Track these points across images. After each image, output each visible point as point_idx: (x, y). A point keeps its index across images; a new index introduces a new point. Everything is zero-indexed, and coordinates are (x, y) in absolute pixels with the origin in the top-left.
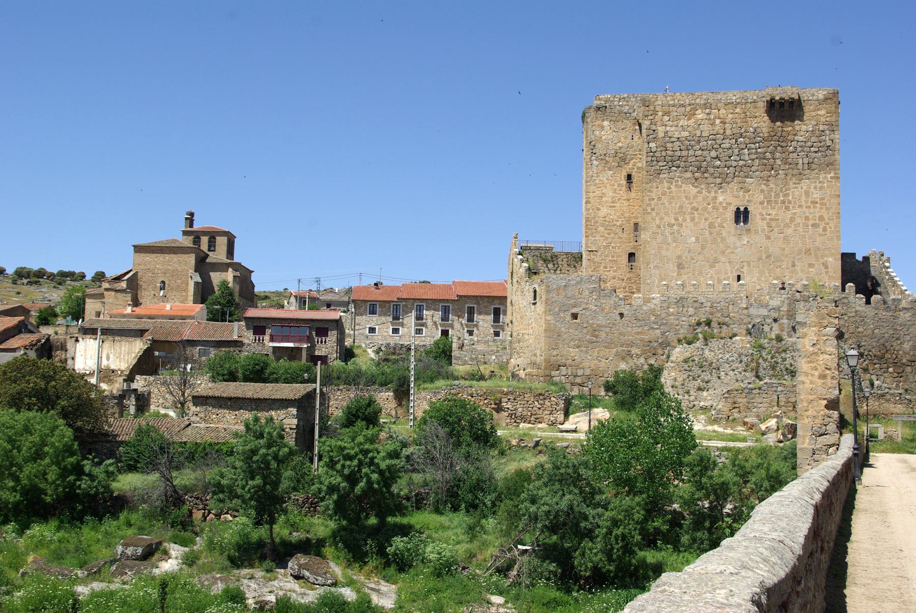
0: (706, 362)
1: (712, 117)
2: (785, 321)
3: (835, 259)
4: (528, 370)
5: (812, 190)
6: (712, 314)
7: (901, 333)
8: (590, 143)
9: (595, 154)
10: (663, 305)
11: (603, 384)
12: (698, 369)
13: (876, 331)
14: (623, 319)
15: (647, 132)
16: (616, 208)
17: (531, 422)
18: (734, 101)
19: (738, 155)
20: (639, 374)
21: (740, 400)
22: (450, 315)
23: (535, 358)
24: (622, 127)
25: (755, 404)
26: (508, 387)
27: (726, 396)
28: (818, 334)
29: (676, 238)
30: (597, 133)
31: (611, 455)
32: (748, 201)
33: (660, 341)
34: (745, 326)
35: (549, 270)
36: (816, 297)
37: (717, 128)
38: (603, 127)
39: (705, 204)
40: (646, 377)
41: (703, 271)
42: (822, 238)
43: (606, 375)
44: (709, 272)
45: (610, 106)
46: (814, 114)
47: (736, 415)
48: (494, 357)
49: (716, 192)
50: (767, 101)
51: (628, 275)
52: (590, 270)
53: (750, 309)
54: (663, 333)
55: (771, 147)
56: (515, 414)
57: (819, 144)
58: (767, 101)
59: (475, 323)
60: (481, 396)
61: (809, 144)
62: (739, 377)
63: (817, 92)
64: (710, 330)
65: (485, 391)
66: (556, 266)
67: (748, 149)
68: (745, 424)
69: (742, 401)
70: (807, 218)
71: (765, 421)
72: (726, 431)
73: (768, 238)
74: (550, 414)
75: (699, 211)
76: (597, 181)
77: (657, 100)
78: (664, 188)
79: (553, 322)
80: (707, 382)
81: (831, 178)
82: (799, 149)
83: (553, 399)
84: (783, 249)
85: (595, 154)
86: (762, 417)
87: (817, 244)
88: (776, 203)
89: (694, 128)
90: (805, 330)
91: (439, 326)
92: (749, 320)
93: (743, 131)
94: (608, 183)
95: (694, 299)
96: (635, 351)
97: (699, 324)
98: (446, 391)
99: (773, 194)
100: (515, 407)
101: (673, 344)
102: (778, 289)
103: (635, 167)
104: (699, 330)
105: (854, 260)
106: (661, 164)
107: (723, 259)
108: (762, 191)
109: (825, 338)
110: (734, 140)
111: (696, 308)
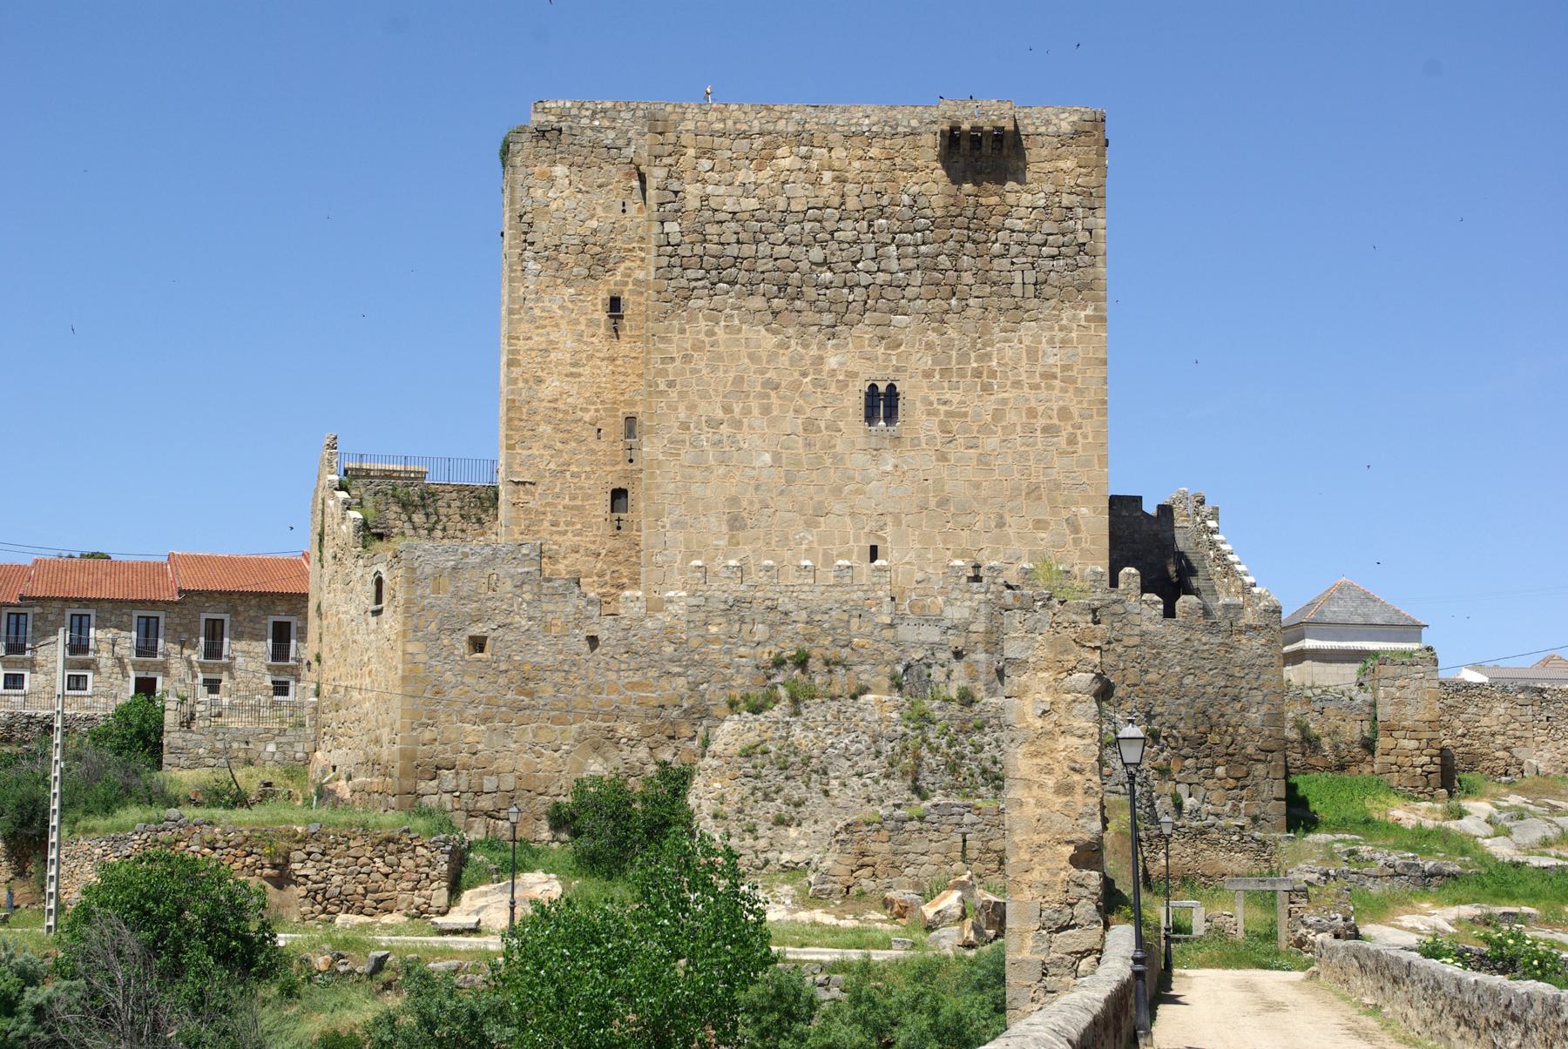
0: (796, 754)
1: (814, 164)
2: (981, 656)
5: (1044, 345)
7: (1244, 683)
8: (521, 217)
11: (547, 813)
13: (1188, 680)
14: (597, 650)
15: (658, 196)
16: (583, 378)
18: (865, 129)
19: (873, 259)
20: (635, 785)
21: (875, 847)
22: (161, 641)
23: (376, 749)
24: (600, 181)
25: (910, 856)
26: (308, 822)
27: (842, 836)
32: (897, 369)
33: (686, 705)
34: (888, 669)
35: (415, 528)
37: (826, 192)
38: (551, 180)
39: (796, 374)
40: (651, 792)
42: (1066, 460)
43: (553, 790)
44: (803, 538)
45: (571, 128)
46: (1048, 166)
47: (867, 884)
48: (271, 748)
49: (821, 346)
51: (610, 544)
52: (516, 529)
53: (900, 628)
54: (693, 686)
55: (951, 243)
56: (325, 890)
57: (1061, 239)
58: (942, 131)
59: (225, 660)
60: (236, 847)
61: (1038, 238)
62: (874, 791)
63: (1057, 116)
64: (805, 679)
65: (246, 833)
66: (433, 519)
67: (898, 247)
68: (887, 904)
70: (1032, 413)
72: (842, 923)
73: (943, 458)
74: (413, 889)
75: (782, 391)
76: (537, 312)
77: (683, 119)
78: (699, 332)
79: (422, 658)
80: (797, 805)
81: (1088, 319)
82: (1015, 249)
84: (978, 486)
87: (1054, 474)
89: (771, 189)
90: (1024, 677)
91: (130, 668)
93: (885, 200)
94: (562, 317)
95: (769, 603)
96: (625, 729)
97: (779, 663)
98: (144, 836)
99: (954, 353)
100: (323, 874)
101: (716, 712)
103: (630, 280)
104: (778, 679)
105: (1139, 514)
106: (691, 274)
107: (837, 507)
108: (929, 346)
109: (1070, 697)
110: (865, 223)
111: (772, 626)
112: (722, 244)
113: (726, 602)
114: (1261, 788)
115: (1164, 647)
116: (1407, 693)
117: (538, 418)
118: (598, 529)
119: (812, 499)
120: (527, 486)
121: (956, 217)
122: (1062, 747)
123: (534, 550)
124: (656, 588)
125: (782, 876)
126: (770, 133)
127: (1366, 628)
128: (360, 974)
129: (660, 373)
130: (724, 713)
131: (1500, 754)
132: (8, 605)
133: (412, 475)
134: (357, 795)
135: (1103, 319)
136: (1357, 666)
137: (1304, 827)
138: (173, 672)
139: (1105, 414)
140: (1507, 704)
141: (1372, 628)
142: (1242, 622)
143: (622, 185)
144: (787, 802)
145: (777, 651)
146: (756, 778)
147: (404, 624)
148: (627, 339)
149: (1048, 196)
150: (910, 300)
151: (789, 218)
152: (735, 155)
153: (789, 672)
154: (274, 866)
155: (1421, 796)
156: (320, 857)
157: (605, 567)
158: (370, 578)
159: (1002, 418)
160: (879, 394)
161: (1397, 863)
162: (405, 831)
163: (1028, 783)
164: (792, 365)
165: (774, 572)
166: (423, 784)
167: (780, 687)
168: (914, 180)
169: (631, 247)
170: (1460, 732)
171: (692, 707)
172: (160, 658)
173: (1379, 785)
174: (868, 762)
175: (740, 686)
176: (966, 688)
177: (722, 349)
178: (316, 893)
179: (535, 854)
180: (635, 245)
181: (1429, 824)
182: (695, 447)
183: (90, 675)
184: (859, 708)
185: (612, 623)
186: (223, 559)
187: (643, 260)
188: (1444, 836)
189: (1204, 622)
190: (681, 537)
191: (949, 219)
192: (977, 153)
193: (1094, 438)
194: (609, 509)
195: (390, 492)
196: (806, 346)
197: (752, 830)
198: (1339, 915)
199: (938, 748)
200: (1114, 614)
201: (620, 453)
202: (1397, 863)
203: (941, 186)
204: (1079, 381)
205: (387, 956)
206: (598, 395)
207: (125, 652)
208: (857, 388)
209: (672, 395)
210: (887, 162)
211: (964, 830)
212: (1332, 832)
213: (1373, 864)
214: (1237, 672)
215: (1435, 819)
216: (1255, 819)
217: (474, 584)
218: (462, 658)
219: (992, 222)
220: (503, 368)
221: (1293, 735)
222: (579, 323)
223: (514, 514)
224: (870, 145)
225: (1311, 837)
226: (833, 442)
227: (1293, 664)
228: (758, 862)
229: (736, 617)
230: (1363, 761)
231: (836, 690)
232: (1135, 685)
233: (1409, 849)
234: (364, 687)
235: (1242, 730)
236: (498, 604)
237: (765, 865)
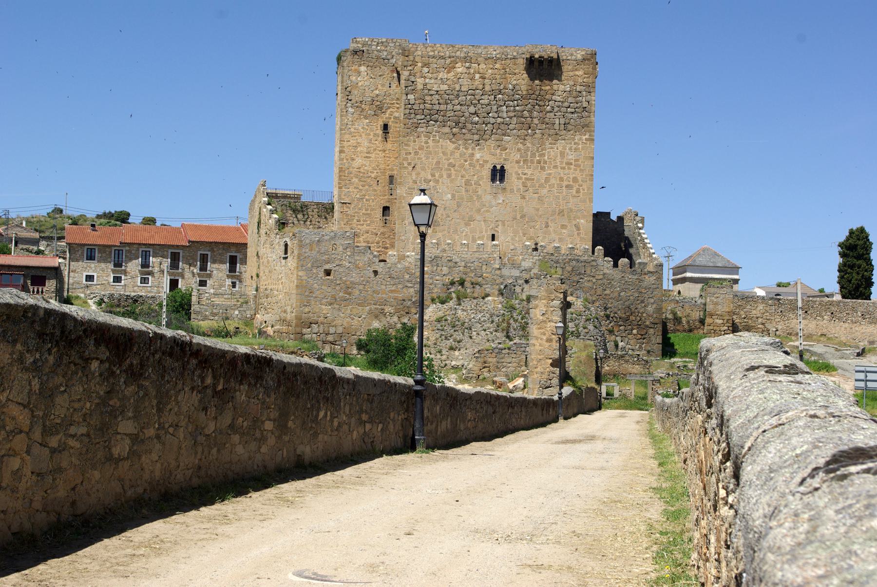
1: (472, 71)
3: (587, 221)
4: (277, 327)
5: (567, 150)
7: (646, 295)
8: (346, 88)
9: (351, 100)
11: (356, 343)
14: (377, 276)
15: (405, 83)
18: (494, 56)
19: (496, 112)
20: (392, 332)
21: (490, 360)
22: (181, 263)
23: (285, 315)
24: (380, 74)
27: (476, 355)
32: (505, 160)
33: (413, 300)
34: (498, 287)
35: (298, 221)
37: (477, 83)
38: (359, 73)
39: (462, 161)
42: (575, 200)
45: (368, 50)
46: (571, 74)
47: (486, 375)
48: (237, 312)
49: (473, 149)
51: (382, 230)
52: (342, 223)
53: (503, 270)
55: (529, 106)
57: (576, 105)
59: (208, 272)
61: (566, 104)
62: (490, 337)
63: (576, 52)
64: (463, 290)
66: (306, 217)
67: (507, 107)
68: (494, 383)
70: (561, 179)
73: (523, 197)
75: (456, 168)
76: (352, 130)
77: (417, 50)
78: (421, 142)
80: (459, 342)
82: (556, 109)
84: (538, 210)
85: (351, 100)
87: (570, 205)
92: (501, 280)
93: (502, 87)
94: (363, 132)
95: (449, 258)
96: (388, 309)
97: (452, 283)
99: (529, 153)
103: (392, 117)
104: (452, 290)
106: (418, 117)
107: (478, 217)
108: (519, 150)
109: (552, 309)
110: (493, 97)
111: (450, 268)
114: (652, 339)
115: (613, 280)
116: (719, 300)
117: (352, 175)
118: (377, 223)
119: (468, 214)
122: (548, 326)
124: (402, 250)
125: (452, 371)
126: (453, 57)
129: (404, 159)
131: (760, 326)
132: (115, 246)
134: (276, 334)
135: (593, 140)
136: (700, 286)
137: (670, 355)
138: (186, 277)
139: (592, 181)
140: (763, 305)
141: (717, 268)
142: (646, 270)
144: (455, 341)
145: (452, 278)
147: (298, 264)
148: (391, 142)
150: (511, 130)
151: (461, 94)
153: (456, 287)
158: (282, 244)
159: (549, 181)
160: (497, 170)
163: (537, 338)
165: (451, 245)
166: (305, 330)
167: (453, 293)
170: (743, 316)
172: (180, 271)
175: (436, 292)
177: (431, 149)
179: (351, 360)
180: (394, 101)
183: (150, 277)
186: (206, 226)
187: (398, 108)
189: (630, 270)
191: (529, 96)
192: (541, 68)
196: (467, 149)
197: (440, 352)
203: (526, 81)
204: (582, 166)
206: (378, 166)
208: (488, 167)
212: (682, 358)
214: (643, 291)
216: (649, 352)
220: (337, 154)
221: (670, 316)
223: (341, 216)
224: (496, 63)
226: (477, 190)
227: (681, 283)
228: (442, 365)
230: (699, 328)
231: (476, 295)
232: (600, 295)
235: (644, 315)
236: (337, 256)
237: (445, 366)
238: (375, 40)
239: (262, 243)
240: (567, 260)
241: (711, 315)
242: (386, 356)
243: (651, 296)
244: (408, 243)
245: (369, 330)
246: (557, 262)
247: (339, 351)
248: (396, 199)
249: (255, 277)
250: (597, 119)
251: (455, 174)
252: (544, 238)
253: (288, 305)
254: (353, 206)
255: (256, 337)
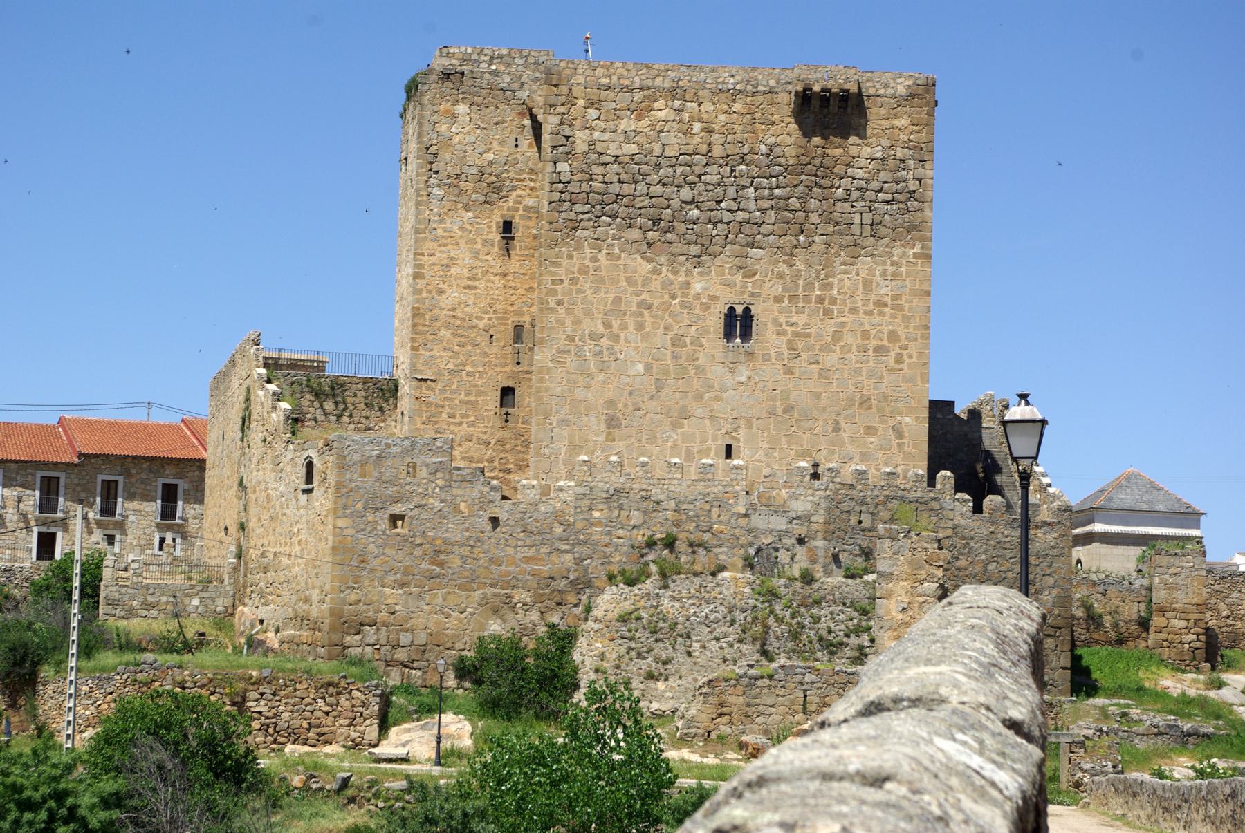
0: (664, 621)
1: (686, 117)
2: (820, 543)
3: (917, 419)
4: (288, 632)
5: (878, 278)
6: (677, 524)
7: (1038, 570)
8: (427, 148)
9: (436, 172)
10: (579, 503)
11: (453, 665)
12: (647, 635)
13: (992, 567)
14: (498, 529)
15: (552, 140)
16: (478, 291)
17: (310, 742)
18: (730, 87)
19: (734, 200)
20: (529, 643)
21: (732, 699)
22: (61, 500)
23: (305, 607)
24: (496, 119)
25: (761, 708)
26: (261, 668)
27: (704, 690)
28: (911, 593)
29: (605, 364)
30: (443, 128)
31: (522, 798)
32: (752, 295)
33: (572, 577)
34: (742, 551)
35: (325, 415)
36: (909, 532)
37: (696, 140)
38: (454, 117)
39: (666, 297)
40: (543, 650)
41: (658, 435)
42: (893, 376)
43: (459, 645)
44: (669, 437)
45: (472, 72)
46: (885, 124)
47: (724, 729)
48: (196, 602)
49: (688, 273)
50: (797, 92)
51: (500, 434)
52: (419, 420)
53: (753, 517)
54: (579, 561)
55: (801, 187)
56: (276, 725)
57: (895, 187)
58: (797, 92)
59: (118, 518)
60: (202, 687)
61: (875, 185)
62: (729, 653)
63: (894, 80)
64: (672, 558)
65: (210, 676)
66: (342, 406)
67: (756, 189)
68: (742, 746)
69: (736, 701)
70: (866, 335)
71: (779, 742)
72: (705, 761)
73: (789, 371)
74: (349, 725)
75: (654, 311)
76: (440, 232)
77: (575, 74)
78: (584, 258)
79: (350, 532)
80: (665, 663)
81: (916, 256)
82: (855, 194)
83: (356, 693)
84: (818, 396)
85: (436, 172)
86: (774, 734)
87: (883, 387)
88: (807, 300)
89: (648, 137)
90: (891, 585)
91: (33, 523)
92: (750, 538)
93: (746, 149)
94: (462, 237)
95: (643, 493)
96: (520, 596)
97: (651, 544)
98: (125, 676)
99: (801, 282)
100: (274, 711)
101: (597, 583)
102: (808, 478)
103: (521, 206)
104: (650, 557)
105: (951, 416)
106: (578, 208)
107: (698, 411)
108: (780, 276)
109: (921, 599)
110: (728, 169)
111: (646, 512)
112: (606, 183)
113: (607, 492)
115: (972, 538)
117: (439, 324)
118: (489, 422)
120: (429, 382)
121: (806, 165)
123: (446, 443)
124: (544, 476)
126: (649, 88)
127: (1149, 514)
128: (329, 791)
130: (603, 585)
133: (315, 364)
134: (286, 645)
135: (928, 257)
136: (1135, 551)
139: (928, 338)
143: (515, 123)
144: (656, 661)
145: (650, 533)
146: (631, 640)
147: (335, 503)
148: (517, 258)
149: (884, 149)
150: (765, 236)
152: (618, 107)
154: (233, 704)
155: (1188, 668)
156: (271, 697)
157: (494, 454)
159: (840, 339)
160: (736, 316)
161: (1161, 724)
162: (343, 677)
164: (663, 289)
168: (771, 132)
169: (522, 177)
170: (1224, 614)
171: (577, 579)
172: (60, 515)
173: (1154, 659)
174: (724, 629)
176: (807, 569)
177: (603, 273)
178: (268, 726)
180: (525, 176)
181: (1192, 693)
182: (579, 357)
184: (717, 583)
185: (512, 507)
187: (532, 189)
188: (1202, 703)
190: (565, 433)
193: (918, 358)
194: (498, 404)
195: (305, 382)
196: (675, 273)
198: (1109, 763)
199: (783, 619)
200: (931, 510)
201: (509, 356)
202: (1161, 724)
204: (907, 309)
205: (350, 777)
207: (28, 508)
209: (561, 312)
210: (748, 116)
211: (805, 687)
212: (1110, 696)
213: (1140, 724)
215: (1197, 689)
217: (394, 471)
218: (384, 532)
219: (836, 170)
221: (1079, 612)
222: (476, 243)
223: (417, 407)
225: (1091, 701)
226: (696, 356)
227: (1083, 545)
229: (616, 505)
230: (1139, 636)
231: (698, 568)
233: (1171, 712)
234: (293, 554)
236: (415, 488)
238: (486, 52)
239: (255, 460)
240: (880, 499)
241: (1163, 611)
242: (517, 691)
243: (1048, 572)
244: (557, 462)
245: (481, 639)
246: (862, 502)
247: (420, 681)
248: (528, 372)
249: (233, 530)
250: (938, 216)
251: (653, 323)
252: (832, 452)
253: (314, 588)
254: (439, 386)
255: (242, 652)
